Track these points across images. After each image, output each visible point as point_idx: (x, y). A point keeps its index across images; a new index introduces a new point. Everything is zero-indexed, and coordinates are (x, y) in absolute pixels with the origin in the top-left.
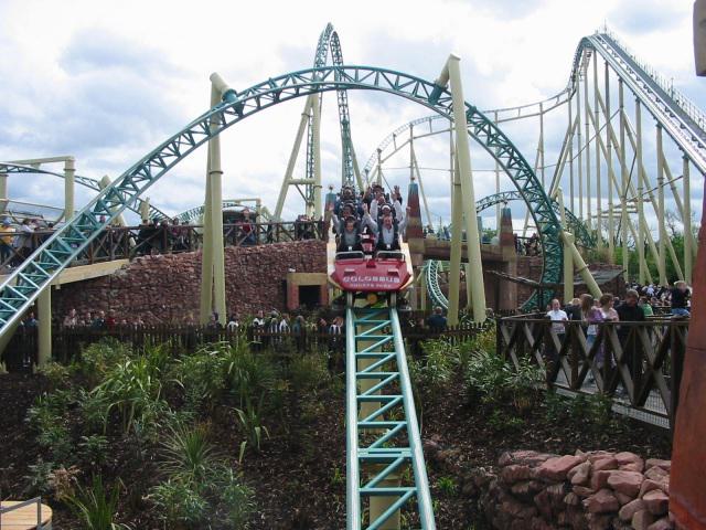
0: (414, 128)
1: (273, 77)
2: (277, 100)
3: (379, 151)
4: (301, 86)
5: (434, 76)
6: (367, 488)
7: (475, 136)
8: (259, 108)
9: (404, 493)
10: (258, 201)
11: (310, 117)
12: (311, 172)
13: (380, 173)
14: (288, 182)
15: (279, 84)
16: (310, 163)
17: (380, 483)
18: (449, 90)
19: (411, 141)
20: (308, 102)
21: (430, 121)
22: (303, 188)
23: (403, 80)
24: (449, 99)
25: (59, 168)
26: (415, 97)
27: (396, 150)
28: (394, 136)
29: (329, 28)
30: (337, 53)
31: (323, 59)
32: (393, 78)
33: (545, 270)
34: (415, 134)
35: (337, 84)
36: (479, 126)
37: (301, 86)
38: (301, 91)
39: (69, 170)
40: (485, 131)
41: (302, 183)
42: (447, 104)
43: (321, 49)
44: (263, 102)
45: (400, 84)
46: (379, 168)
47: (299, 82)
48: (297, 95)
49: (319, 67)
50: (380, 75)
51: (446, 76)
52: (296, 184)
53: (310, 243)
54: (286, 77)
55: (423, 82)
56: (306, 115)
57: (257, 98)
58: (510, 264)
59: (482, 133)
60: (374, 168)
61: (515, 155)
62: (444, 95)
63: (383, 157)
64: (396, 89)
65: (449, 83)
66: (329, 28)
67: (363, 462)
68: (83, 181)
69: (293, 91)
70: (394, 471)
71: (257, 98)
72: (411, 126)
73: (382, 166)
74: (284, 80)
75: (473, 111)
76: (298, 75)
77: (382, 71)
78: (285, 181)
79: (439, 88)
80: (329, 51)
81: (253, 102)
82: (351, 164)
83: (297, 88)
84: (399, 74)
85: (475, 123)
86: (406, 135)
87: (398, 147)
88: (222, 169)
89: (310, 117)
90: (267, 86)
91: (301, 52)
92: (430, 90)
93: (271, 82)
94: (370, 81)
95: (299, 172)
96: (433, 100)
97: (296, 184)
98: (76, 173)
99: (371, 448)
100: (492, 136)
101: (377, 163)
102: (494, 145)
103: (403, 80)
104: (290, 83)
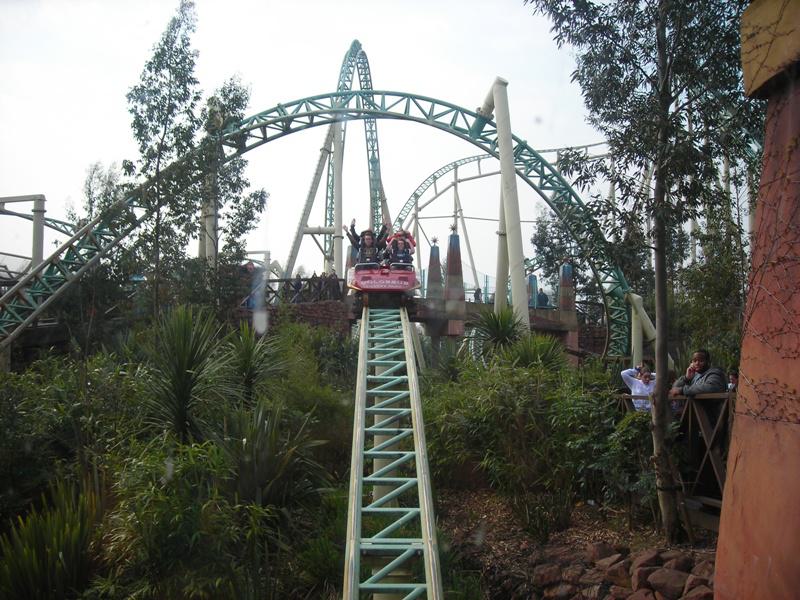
0: (459, 169)
1: (283, 103)
2: (287, 131)
3: (417, 196)
4: (316, 114)
5: (475, 102)
6: (367, 584)
7: (525, 178)
8: (265, 140)
9: (411, 590)
10: (268, 254)
11: (332, 151)
12: (331, 219)
13: (417, 223)
14: (304, 229)
15: (290, 111)
16: (329, 209)
17: (385, 578)
18: (494, 120)
19: (455, 184)
20: (330, 131)
21: (479, 160)
22: (321, 238)
23: (439, 109)
24: (494, 132)
25: (28, 208)
26: (453, 130)
27: (438, 195)
28: (435, 178)
29: (356, 46)
30: (365, 78)
31: (348, 84)
32: (426, 106)
33: (610, 341)
34: (460, 177)
35: (359, 112)
36: (530, 166)
37: (316, 114)
38: (316, 119)
39: (39, 211)
40: (537, 171)
41: (320, 232)
42: (492, 137)
43: (345, 73)
44: (270, 132)
45: (435, 114)
46: (416, 216)
47: (313, 108)
48: (311, 125)
49: (344, 94)
50: (460, 114)
51: (490, 106)
52: (313, 233)
53: (326, 305)
54: (299, 103)
55: (464, 111)
56: (326, 151)
57: (263, 128)
58: (570, 333)
59: (533, 173)
60: (410, 217)
61: (573, 199)
62: (488, 127)
63: (421, 203)
64: (430, 120)
65: (494, 113)
66: (356, 46)
67: (418, 534)
68: (55, 225)
69: (306, 119)
70: (400, 567)
71: (263, 128)
72: (456, 167)
73: (420, 214)
74: (296, 106)
75: (523, 146)
76: (311, 100)
77: (414, 97)
78: (300, 229)
79: (484, 118)
80: (356, 73)
81: (257, 132)
82: (380, 210)
83: (312, 115)
84: (434, 102)
85: (525, 161)
86: (449, 178)
87: (438, 192)
88: (46, 208)
89: (332, 151)
90: (275, 114)
91: (323, 79)
92: (472, 120)
93: (280, 108)
94: (400, 109)
95: (317, 220)
96: (475, 135)
97: (313, 233)
98: (46, 215)
99: (374, 539)
100: (546, 177)
101: (413, 211)
102: (548, 188)
103: (439, 109)
104: (303, 110)
